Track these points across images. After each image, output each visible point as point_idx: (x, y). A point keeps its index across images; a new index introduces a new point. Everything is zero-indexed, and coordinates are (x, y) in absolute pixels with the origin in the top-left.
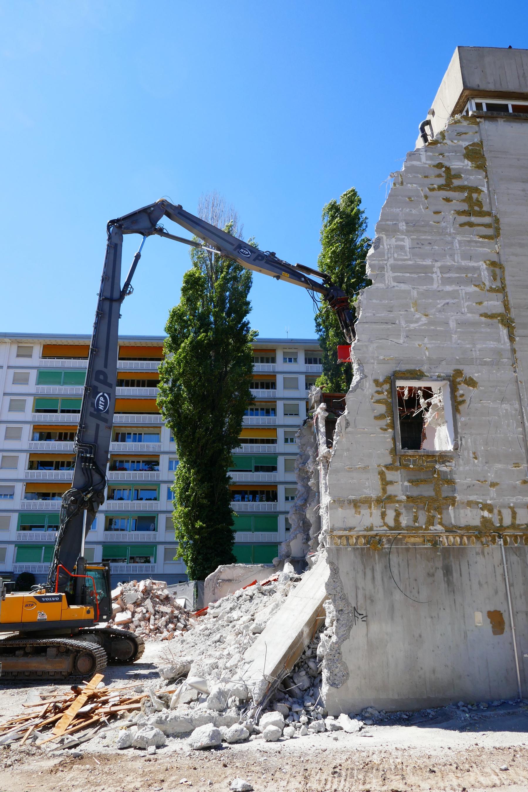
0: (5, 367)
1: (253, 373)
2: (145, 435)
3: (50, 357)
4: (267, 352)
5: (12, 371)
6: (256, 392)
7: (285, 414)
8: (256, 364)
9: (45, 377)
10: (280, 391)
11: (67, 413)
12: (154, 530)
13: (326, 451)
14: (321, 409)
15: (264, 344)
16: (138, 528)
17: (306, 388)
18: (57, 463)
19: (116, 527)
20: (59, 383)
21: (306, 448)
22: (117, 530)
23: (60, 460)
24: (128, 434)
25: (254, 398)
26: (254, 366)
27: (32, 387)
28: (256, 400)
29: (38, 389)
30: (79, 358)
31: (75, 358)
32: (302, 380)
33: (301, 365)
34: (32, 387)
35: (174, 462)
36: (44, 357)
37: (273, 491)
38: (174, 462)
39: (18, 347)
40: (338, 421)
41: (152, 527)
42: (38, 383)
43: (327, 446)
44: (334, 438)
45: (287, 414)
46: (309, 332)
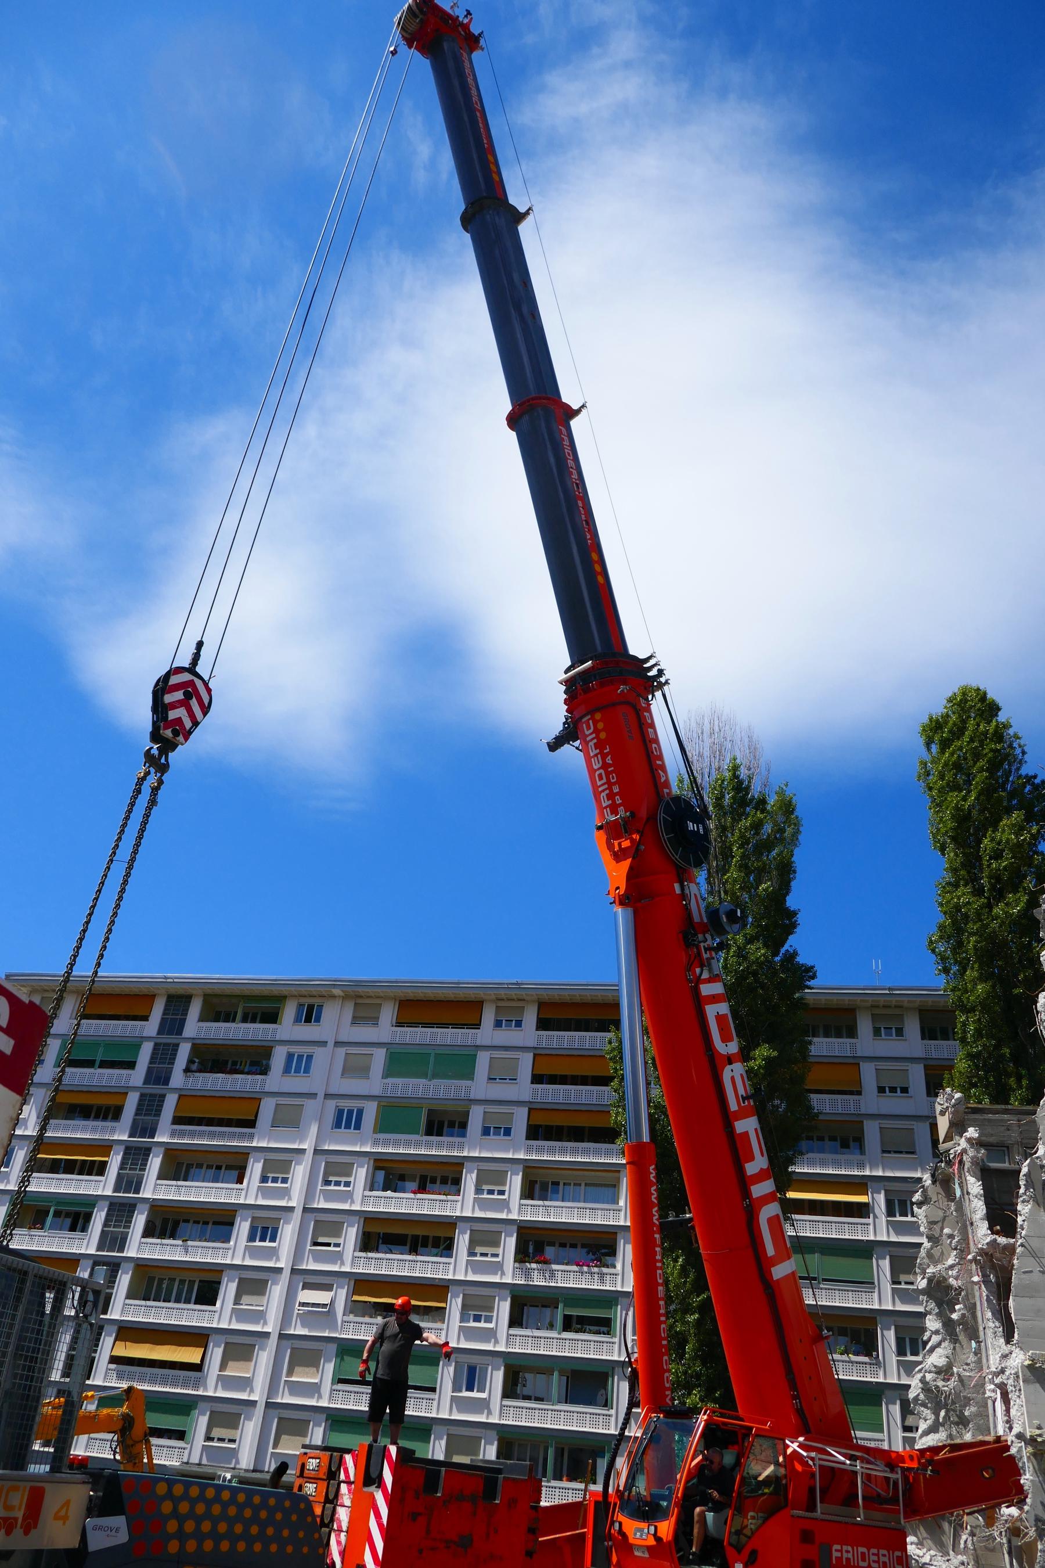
0: (331, 1044)
1: (811, 1060)
2: (589, 1189)
3: (411, 1025)
4: (840, 1018)
5: (342, 1051)
6: (820, 1102)
7: (884, 1152)
8: (815, 1040)
9: (401, 1062)
10: (870, 1101)
11: (139, 1365)
12: (606, 1405)
13: (988, 1239)
14: (969, 1140)
15: (403, 1166)
16: (571, 1398)
17: (929, 1094)
18: (415, 1238)
19: (526, 1391)
20: (425, 1075)
21: (942, 1229)
22: (527, 1398)
23: (420, 1232)
24: (553, 1183)
25: (817, 1115)
26: (810, 1043)
27: (375, 1083)
28: (821, 1117)
29: (385, 1087)
30: (462, 1026)
31: (456, 1026)
32: (917, 1077)
33: (912, 1042)
34: (375, 1083)
35: (907, 1340)
36: (399, 1024)
37: (867, 1331)
38: (907, 1340)
39: (356, 1004)
40: (1025, 1170)
41: (601, 1399)
42: (388, 1073)
43: (991, 1228)
44: (1019, 1207)
45: (889, 1152)
46: (924, 976)
